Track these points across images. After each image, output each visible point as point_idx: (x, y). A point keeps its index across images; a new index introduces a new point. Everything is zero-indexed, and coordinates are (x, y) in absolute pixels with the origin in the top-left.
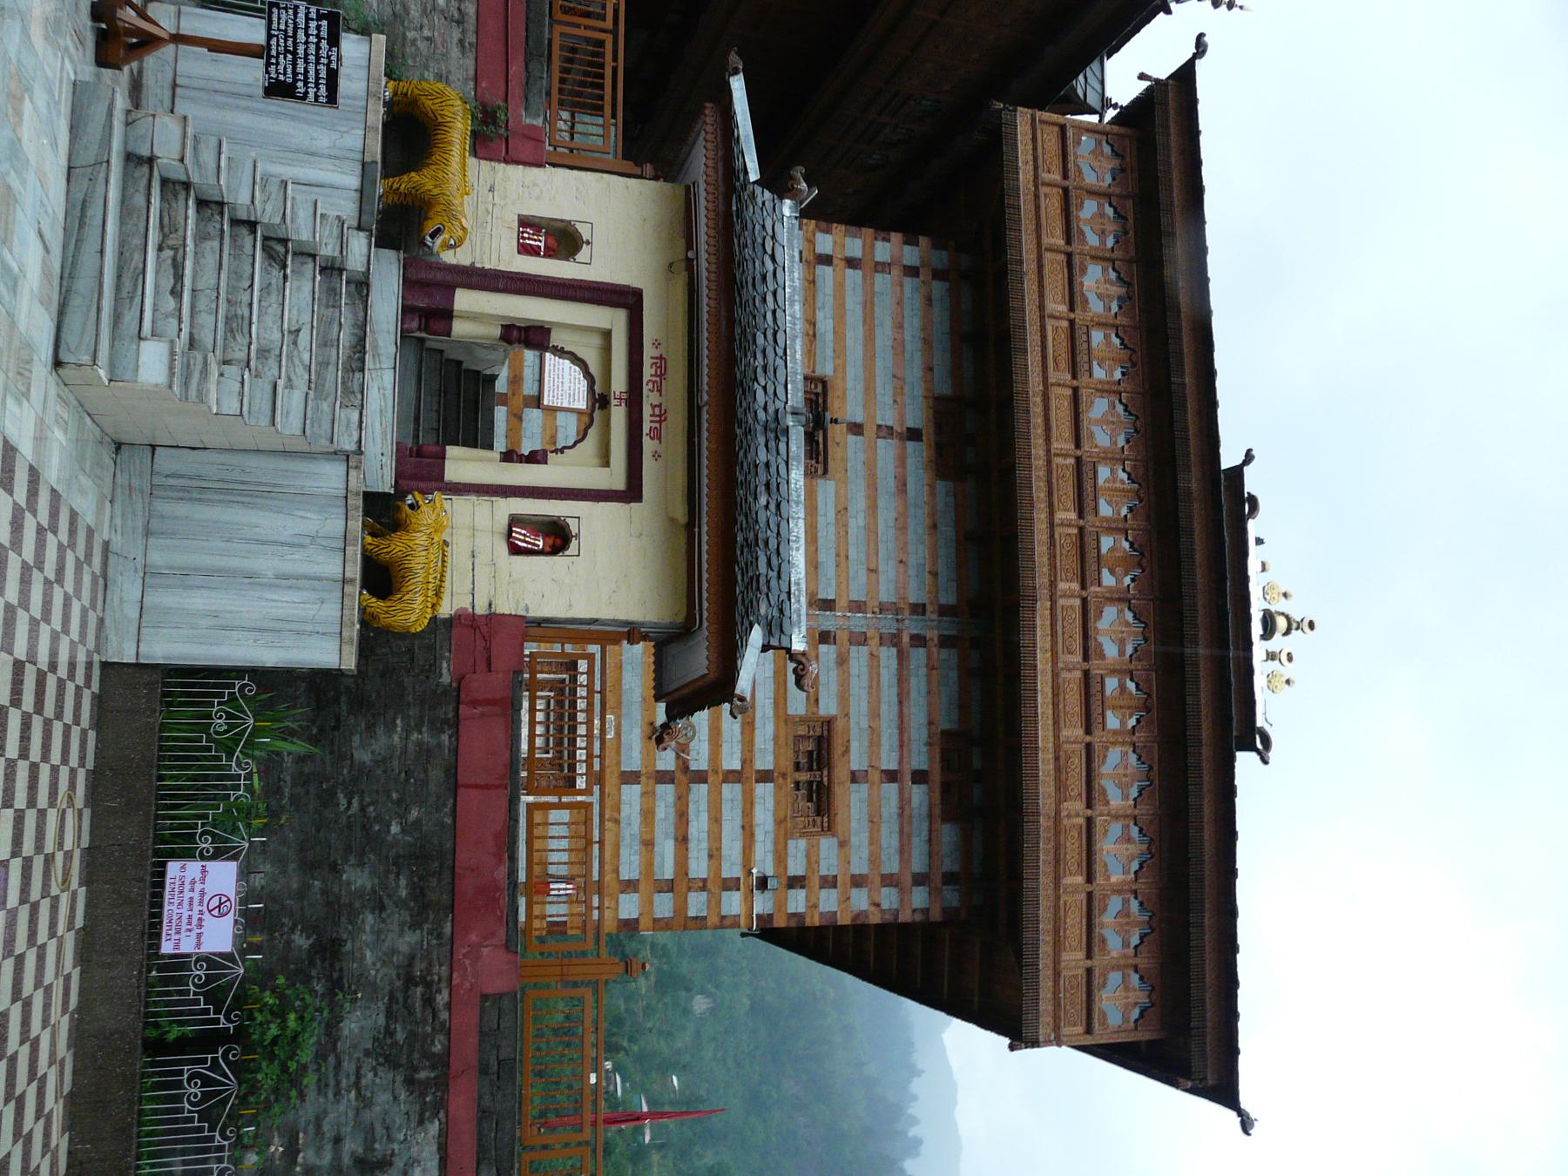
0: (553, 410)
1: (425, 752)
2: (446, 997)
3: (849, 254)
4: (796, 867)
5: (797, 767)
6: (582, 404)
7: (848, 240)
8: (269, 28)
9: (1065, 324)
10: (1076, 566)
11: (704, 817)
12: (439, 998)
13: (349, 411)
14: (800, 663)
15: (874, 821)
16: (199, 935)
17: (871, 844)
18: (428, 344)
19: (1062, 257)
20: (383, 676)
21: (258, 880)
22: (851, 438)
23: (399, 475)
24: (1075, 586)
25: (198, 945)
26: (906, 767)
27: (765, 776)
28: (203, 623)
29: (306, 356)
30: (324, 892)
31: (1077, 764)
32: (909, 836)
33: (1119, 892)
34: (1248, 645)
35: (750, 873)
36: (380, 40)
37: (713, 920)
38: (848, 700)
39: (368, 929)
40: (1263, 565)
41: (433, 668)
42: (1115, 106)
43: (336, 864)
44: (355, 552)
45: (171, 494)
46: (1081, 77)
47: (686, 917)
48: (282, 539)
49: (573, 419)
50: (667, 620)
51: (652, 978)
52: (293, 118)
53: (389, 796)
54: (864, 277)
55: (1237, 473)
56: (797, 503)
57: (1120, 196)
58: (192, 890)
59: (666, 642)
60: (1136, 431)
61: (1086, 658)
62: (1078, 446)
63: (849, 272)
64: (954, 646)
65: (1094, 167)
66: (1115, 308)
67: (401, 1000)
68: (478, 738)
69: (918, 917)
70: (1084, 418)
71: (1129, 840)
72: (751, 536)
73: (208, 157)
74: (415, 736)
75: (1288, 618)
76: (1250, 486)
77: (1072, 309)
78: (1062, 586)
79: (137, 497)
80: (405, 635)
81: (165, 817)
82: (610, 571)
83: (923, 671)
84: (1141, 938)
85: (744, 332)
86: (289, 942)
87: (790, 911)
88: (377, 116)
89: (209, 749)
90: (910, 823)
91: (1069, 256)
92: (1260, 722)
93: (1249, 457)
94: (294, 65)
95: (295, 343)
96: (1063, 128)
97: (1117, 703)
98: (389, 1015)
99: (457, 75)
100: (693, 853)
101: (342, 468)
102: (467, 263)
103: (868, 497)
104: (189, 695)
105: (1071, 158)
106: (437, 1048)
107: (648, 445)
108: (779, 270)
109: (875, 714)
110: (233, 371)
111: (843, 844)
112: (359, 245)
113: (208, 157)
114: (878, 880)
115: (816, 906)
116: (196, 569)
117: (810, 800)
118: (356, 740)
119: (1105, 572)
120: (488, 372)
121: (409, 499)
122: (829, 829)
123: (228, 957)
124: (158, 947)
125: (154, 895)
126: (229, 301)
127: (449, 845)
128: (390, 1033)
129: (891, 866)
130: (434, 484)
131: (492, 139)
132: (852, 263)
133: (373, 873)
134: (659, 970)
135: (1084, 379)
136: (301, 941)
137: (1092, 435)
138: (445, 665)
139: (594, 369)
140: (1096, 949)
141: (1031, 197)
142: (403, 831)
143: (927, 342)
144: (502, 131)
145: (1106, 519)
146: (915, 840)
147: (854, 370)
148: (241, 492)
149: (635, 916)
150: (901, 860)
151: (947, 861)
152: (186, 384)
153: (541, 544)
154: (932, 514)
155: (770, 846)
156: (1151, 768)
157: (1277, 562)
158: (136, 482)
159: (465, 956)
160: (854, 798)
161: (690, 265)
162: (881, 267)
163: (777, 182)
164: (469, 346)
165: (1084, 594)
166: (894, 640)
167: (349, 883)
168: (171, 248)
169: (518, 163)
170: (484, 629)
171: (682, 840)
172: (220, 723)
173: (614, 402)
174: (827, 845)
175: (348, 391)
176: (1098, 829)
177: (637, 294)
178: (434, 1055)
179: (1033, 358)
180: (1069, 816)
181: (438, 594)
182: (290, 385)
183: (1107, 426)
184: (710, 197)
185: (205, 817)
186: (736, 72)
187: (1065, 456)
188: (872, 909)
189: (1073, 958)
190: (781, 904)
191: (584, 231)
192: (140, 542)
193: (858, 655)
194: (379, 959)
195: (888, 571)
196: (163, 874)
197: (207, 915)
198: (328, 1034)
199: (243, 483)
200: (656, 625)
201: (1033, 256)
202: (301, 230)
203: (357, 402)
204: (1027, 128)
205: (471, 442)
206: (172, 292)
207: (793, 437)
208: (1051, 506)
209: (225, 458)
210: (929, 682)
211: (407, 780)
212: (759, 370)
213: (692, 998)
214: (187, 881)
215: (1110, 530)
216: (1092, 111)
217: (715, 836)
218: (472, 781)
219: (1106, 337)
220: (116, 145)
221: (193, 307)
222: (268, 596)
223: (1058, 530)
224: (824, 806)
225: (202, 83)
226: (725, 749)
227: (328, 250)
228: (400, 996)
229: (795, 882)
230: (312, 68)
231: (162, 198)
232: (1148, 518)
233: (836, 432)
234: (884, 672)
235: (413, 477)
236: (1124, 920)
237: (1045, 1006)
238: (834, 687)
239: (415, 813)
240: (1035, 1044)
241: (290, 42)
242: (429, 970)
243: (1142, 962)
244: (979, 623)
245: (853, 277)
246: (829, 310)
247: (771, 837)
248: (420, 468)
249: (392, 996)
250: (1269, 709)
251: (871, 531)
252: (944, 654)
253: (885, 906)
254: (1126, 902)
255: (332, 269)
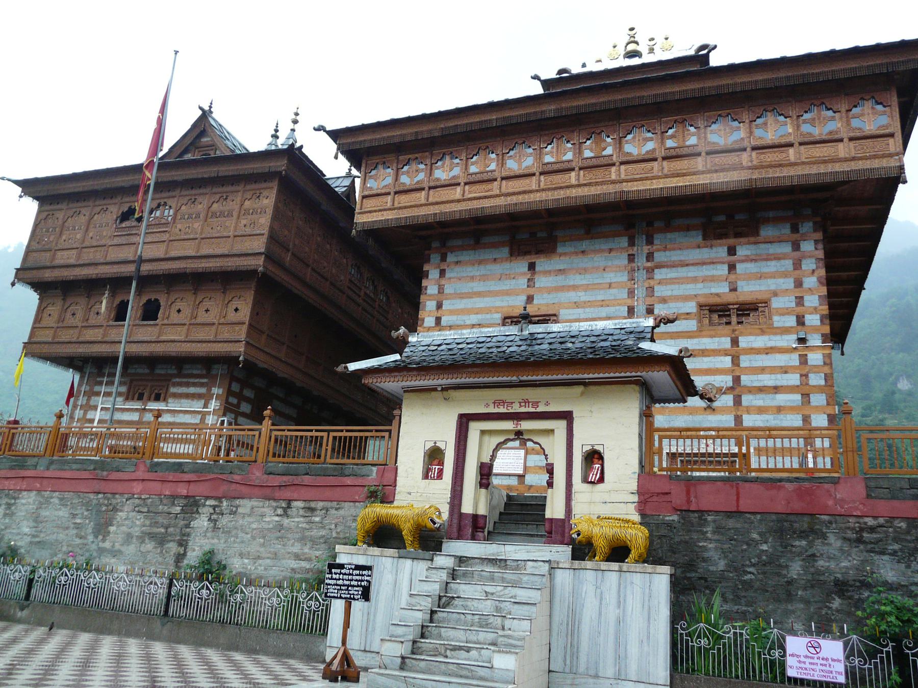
0: (525, 468)
1: (718, 530)
2: (870, 519)
3: (434, 308)
4: (791, 321)
5: (729, 323)
6: (522, 452)
7: (428, 309)
8: (337, 598)
9: (467, 187)
10: (602, 170)
11: (761, 377)
12: (870, 524)
13: (527, 567)
14: (660, 321)
15: (761, 276)
16: (833, 660)
17: (775, 278)
18: (491, 529)
19: (431, 192)
20: (674, 553)
21: (798, 626)
22: (535, 302)
23: (562, 543)
24: (613, 169)
25: (839, 661)
26: (726, 260)
27: (735, 342)
28: (646, 649)
29: (499, 588)
30: (805, 589)
31: (719, 159)
32: (768, 255)
33: (798, 127)
34: (644, 66)
35: (795, 348)
36: (338, 548)
37: (827, 369)
38: (687, 296)
39: (827, 564)
40: (598, 61)
41: (669, 525)
42: (350, 170)
43: (787, 582)
44: (604, 565)
45: (575, 663)
46: (336, 189)
47: (826, 386)
48: (598, 604)
49: (529, 457)
50: (638, 395)
51: (887, 416)
52: (378, 593)
53: (745, 550)
54: (446, 299)
55: (546, 83)
56: (571, 327)
57: (398, 163)
58: (804, 663)
59: (651, 397)
60: (524, 142)
61: (655, 160)
62: (534, 175)
63: (444, 307)
64: (652, 237)
65: (383, 179)
66: (457, 161)
67: (873, 546)
68: (707, 499)
69: (821, 246)
70: (517, 173)
71: (765, 124)
72: (590, 350)
73: (400, 631)
74: (709, 535)
75: (628, 44)
76: (553, 75)
77: (459, 184)
78: (613, 177)
79: (577, 681)
80: (651, 539)
81: (761, 677)
82: (611, 426)
83: (668, 253)
84: (829, 109)
85: (479, 359)
86: (837, 611)
87: (819, 323)
88: (376, 551)
89: (719, 649)
90: (760, 255)
91: (430, 188)
92: (692, 52)
93: (536, 77)
94: (354, 586)
95: (492, 594)
96: (364, 197)
97: (681, 140)
98: (882, 553)
99: (353, 511)
100: (785, 383)
101: (558, 572)
102: (448, 506)
103: (568, 290)
104: (687, 660)
105: (379, 191)
106: (903, 525)
107: (542, 408)
108: (446, 342)
109: (695, 280)
110: (508, 624)
111: (775, 294)
112: (441, 560)
113: (400, 631)
114: (797, 272)
115: (815, 308)
116: (616, 650)
117: (749, 315)
118: (711, 568)
119: (604, 153)
120: (505, 499)
121: (575, 536)
122: (766, 302)
123: (846, 645)
124: (840, 684)
125: (808, 685)
126: (472, 626)
127: (774, 517)
128: (894, 553)
129: (788, 264)
130: (567, 524)
131: (383, 493)
132: (439, 306)
133: (792, 560)
134: (881, 412)
135: (497, 175)
136: (836, 603)
137: (527, 167)
138: (667, 518)
139: (502, 439)
140: (836, 137)
141: (400, 211)
142: (766, 543)
143: (480, 262)
144: (380, 488)
145: (574, 155)
146: (771, 251)
147: (498, 302)
148: (573, 625)
149: (825, 417)
150: (784, 259)
151: (783, 231)
152: (515, 646)
153: (597, 466)
154: (576, 253)
155: (778, 337)
156: (720, 115)
157: (598, 53)
158: (569, 682)
159: (842, 507)
160: (746, 289)
161: (445, 389)
162: (441, 290)
163: (400, 345)
164: (491, 508)
165: (617, 164)
166: (650, 271)
167: (799, 574)
168: (446, 651)
169: (396, 480)
170: (647, 496)
171: (776, 389)
172: (704, 642)
173: (519, 428)
174: (776, 303)
175: (517, 568)
176: (759, 143)
177: (461, 416)
178: (908, 526)
179: (487, 203)
180: (751, 161)
181: (628, 521)
182: (515, 597)
183: (522, 159)
184: (410, 379)
185: (759, 653)
186: (346, 368)
187: (540, 181)
188: (816, 274)
189: (842, 150)
190: (815, 329)
191: (430, 445)
192: (602, 681)
193: (660, 291)
194: (846, 558)
195: (610, 277)
196: (796, 679)
197: (820, 655)
198: (897, 589)
199: (568, 624)
200: (641, 402)
201: (431, 207)
202: (435, 589)
203: (523, 563)
204: (367, 216)
205: (543, 507)
206: (468, 652)
207: (534, 331)
208: (568, 187)
209: (554, 634)
210: (674, 249)
211: (735, 540)
212: (499, 350)
213: (900, 390)
214: (799, 665)
215: (580, 152)
216: (353, 182)
217: (772, 370)
218: (735, 502)
219: (473, 164)
220: (397, 673)
221: (475, 643)
222: (629, 613)
223: (582, 182)
224: (752, 307)
225: (363, 638)
226: (719, 366)
227: (443, 575)
228: (869, 546)
229: (800, 321)
230: (354, 578)
231: (421, 654)
232: (573, 131)
233: (531, 310)
234: (669, 276)
235: (563, 535)
236: (817, 121)
237: (876, 164)
238: (680, 304)
239: (755, 536)
240: (902, 168)
241: (343, 588)
242: (853, 529)
243: (844, 107)
244: (638, 222)
245: (446, 305)
246: (465, 318)
247: (772, 337)
248: (557, 532)
249: (871, 551)
250: (684, 48)
251: (586, 288)
252: (656, 242)
253: (814, 267)
254: (805, 122)
255: (453, 574)
